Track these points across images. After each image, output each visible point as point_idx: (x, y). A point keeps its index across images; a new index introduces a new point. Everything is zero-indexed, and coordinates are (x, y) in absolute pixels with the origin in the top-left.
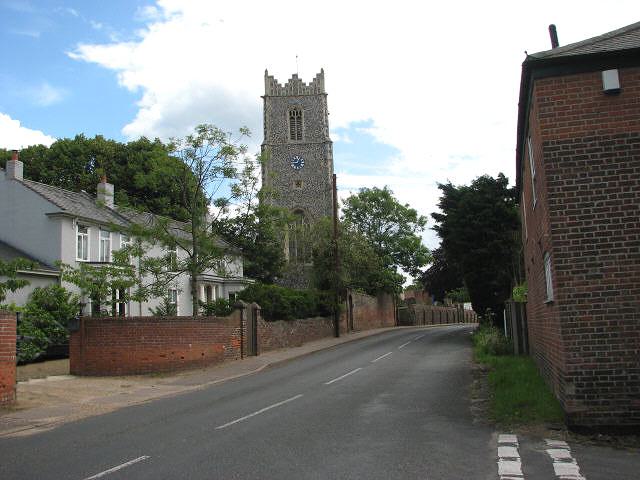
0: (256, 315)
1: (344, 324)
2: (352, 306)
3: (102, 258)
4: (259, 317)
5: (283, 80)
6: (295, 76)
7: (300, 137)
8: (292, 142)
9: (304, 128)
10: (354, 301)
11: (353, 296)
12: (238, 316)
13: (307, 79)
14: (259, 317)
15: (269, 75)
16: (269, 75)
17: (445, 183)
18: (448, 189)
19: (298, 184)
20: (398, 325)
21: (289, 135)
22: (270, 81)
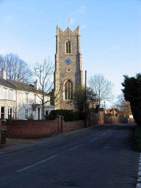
0: (62, 119)
1: (87, 123)
2: (90, 117)
3: (4, 98)
4: (63, 120)
5: (64, 30)
6: (68, 28)
7: (70, 52)
8: (67, 54)
9: (71, 49)
10: (91, 115)
11: (91, 113)
12: (57, 120)
13: (73, 29)
14: (63, 120)
15: (58, 27)
16: (58, 27)
17: (125, 75)
18: (126, 77)
19: (69, 70)
20: (105, 123)
21: (66, 51)
22: (126, 77)
